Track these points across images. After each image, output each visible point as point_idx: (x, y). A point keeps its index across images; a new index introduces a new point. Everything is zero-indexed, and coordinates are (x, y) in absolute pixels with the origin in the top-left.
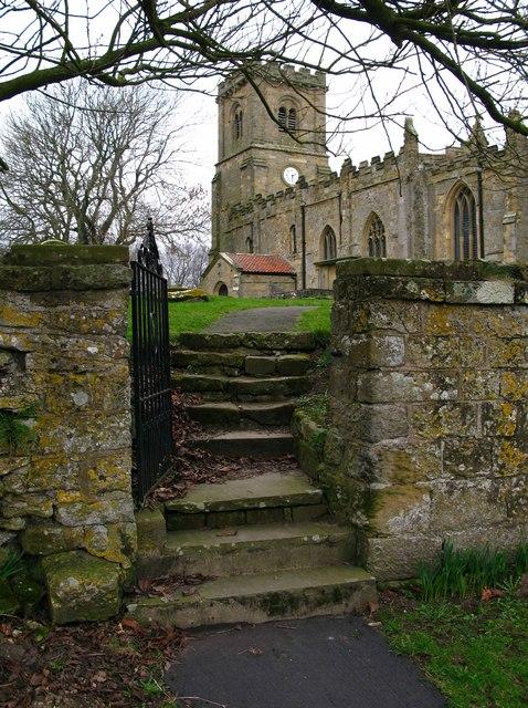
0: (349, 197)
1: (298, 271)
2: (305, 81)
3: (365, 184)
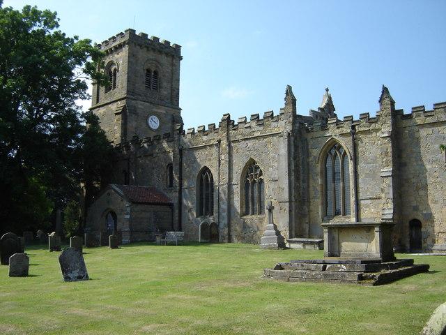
1: (175, 201)
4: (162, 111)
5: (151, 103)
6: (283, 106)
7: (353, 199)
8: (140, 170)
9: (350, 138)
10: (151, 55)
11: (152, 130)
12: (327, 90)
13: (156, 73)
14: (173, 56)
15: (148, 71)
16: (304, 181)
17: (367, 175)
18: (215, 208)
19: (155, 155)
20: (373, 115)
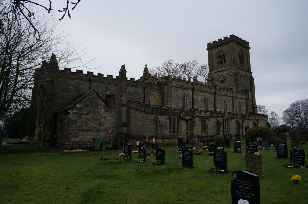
12: (146, 65)
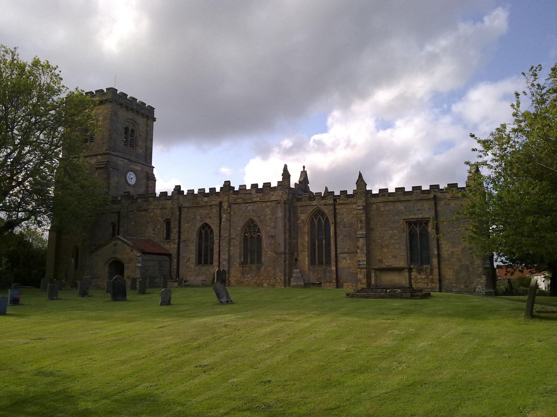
0: (230, 206)
1: (174, 252)
2: (143, 111)
3: (244, 200)
4: (138, 168)
5: (129, 160)
6: (281, 180)
7: (333, 253)
8: (133, 223)
9: (332, 208)
10: (130, 115)
11: (129, 185)
12: (304, 167)
13: (133, 131)
14: (148, 117)
15: (126, 129)
16: (294, 238)
17: (345, 236)
18: (216, 257)
19: (150, 210)
20: (350, 192)
